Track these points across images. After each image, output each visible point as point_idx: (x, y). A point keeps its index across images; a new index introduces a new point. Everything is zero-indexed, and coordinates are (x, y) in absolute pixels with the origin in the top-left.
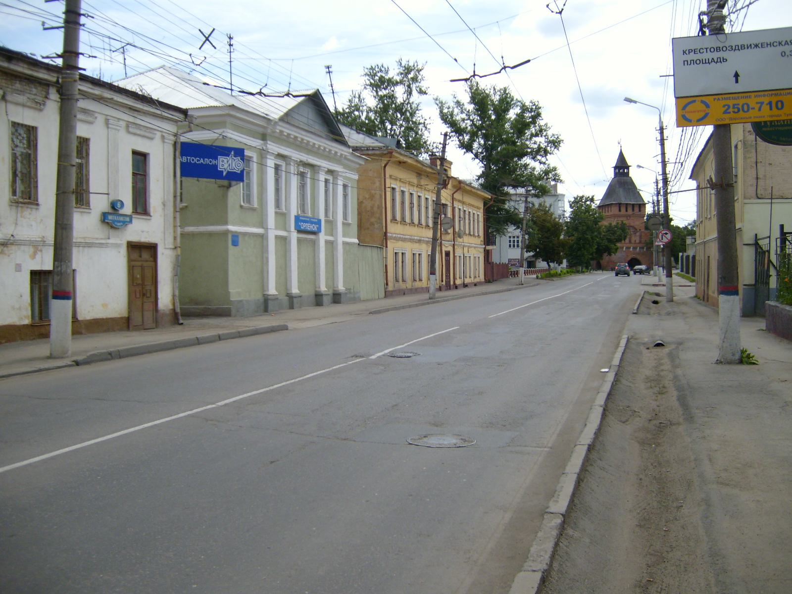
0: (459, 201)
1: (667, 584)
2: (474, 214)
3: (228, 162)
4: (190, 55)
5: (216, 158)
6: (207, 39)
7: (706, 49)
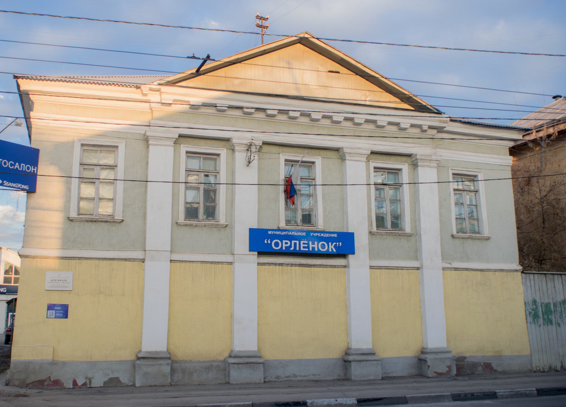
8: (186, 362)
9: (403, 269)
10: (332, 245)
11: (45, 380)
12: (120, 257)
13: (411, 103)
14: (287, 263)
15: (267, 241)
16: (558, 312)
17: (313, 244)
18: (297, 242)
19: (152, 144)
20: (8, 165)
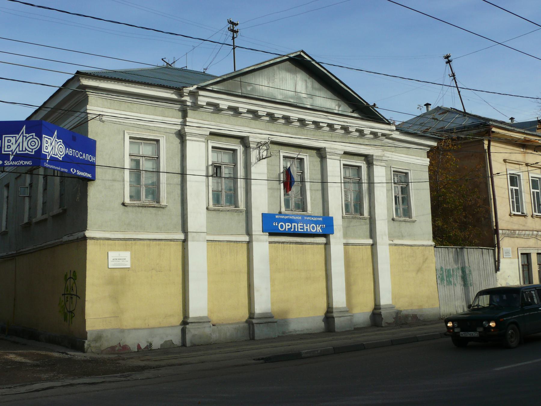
1: (196, 107)
3: (16, 142)
8: (223, 324)
9: (363, 245)
10: (319, 227)
11: (116, 346)
12: (167, 238)
13: (350, 102)
14: (287, 242)
15: (275, 224)
16: (455, 276)
17: (307, 226)
18: (296, 224)
19: (188, 140)
20: (79, 156)
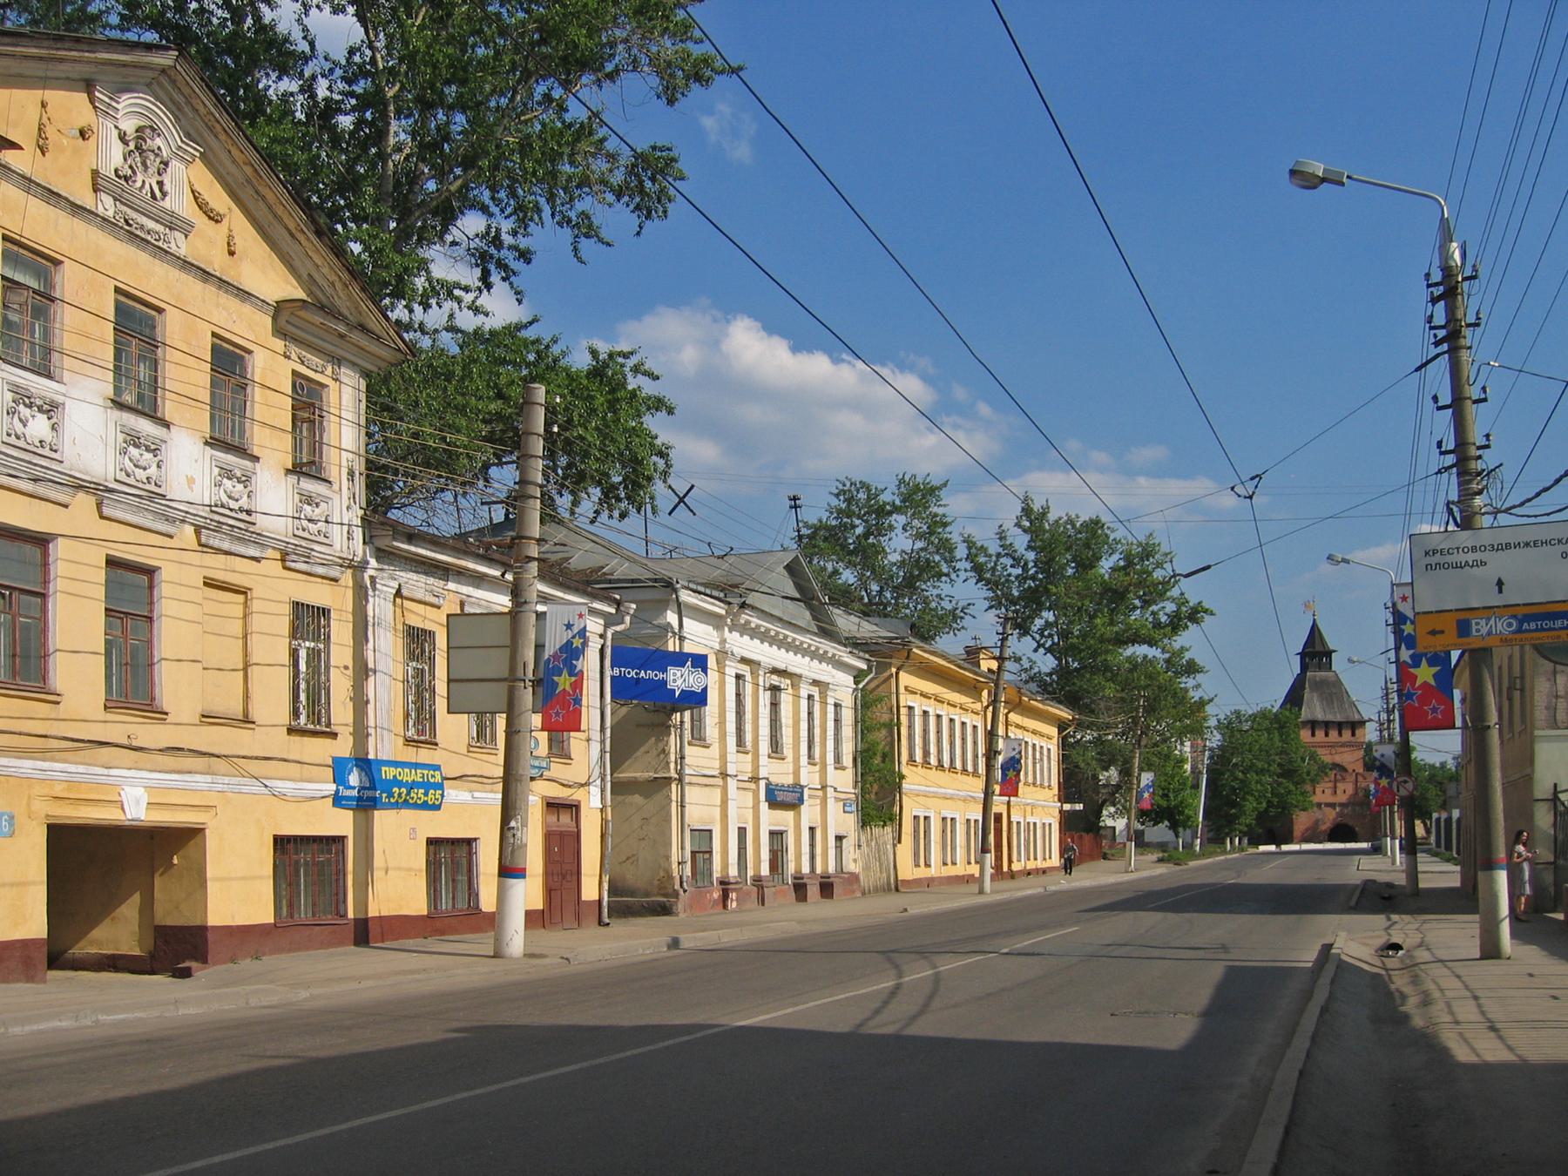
0: (1018, 726)
2: (1041, 747)
4: (709, 544)
5: (665, 671)
6: (681, 500)
7: (1458, 548)
